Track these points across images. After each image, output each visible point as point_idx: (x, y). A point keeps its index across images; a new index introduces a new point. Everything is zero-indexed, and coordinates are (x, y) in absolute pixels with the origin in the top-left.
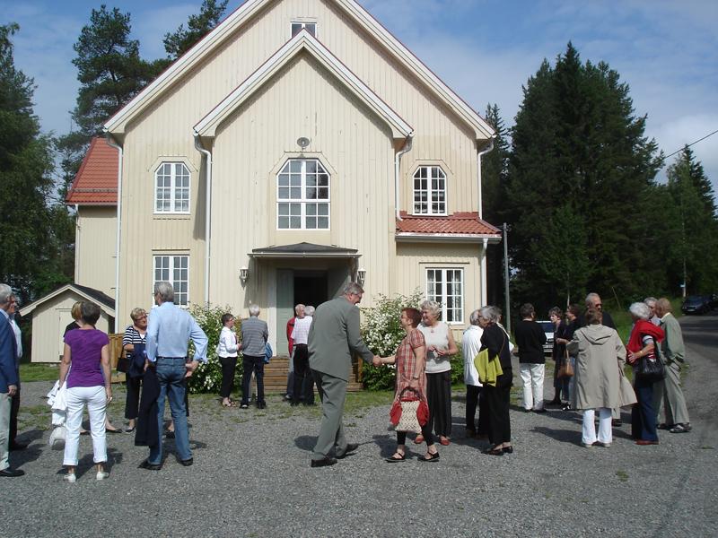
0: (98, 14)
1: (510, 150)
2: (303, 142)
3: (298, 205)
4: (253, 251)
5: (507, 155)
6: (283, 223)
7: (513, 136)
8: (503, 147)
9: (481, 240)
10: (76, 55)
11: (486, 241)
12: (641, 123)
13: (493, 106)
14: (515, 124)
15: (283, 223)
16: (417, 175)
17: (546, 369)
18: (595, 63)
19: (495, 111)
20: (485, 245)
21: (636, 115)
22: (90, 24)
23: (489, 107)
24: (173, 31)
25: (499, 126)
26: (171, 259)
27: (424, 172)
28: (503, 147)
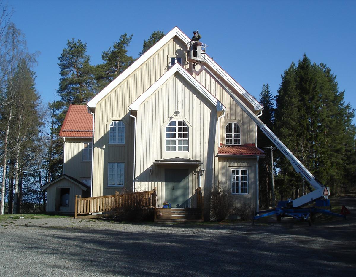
0: (70, 43)
1: (275, 107)
2: (177, 113)
3: (175, 141)
4: (155, 161)
5: (274, 110)
6: (168, 149)
7: (277, 100)
8: (271, 106)
9: (256, 156)
10: (59, 62)
11: (258, 157)
12: (342, 94)
13: (266, 85)
14: (278, 94)
15: (168, 149)
16: (227, 127)
17: (102, 66)
18: (318, 64)
19: (267, 87)
20: (258, 159)
21: (340, 90)
22: (67, 48)
23: (264, 86)
24: (106, 50)
25: (269, 95)
26: (240, 171)
27: (231, 125)
28: (271, 106)
